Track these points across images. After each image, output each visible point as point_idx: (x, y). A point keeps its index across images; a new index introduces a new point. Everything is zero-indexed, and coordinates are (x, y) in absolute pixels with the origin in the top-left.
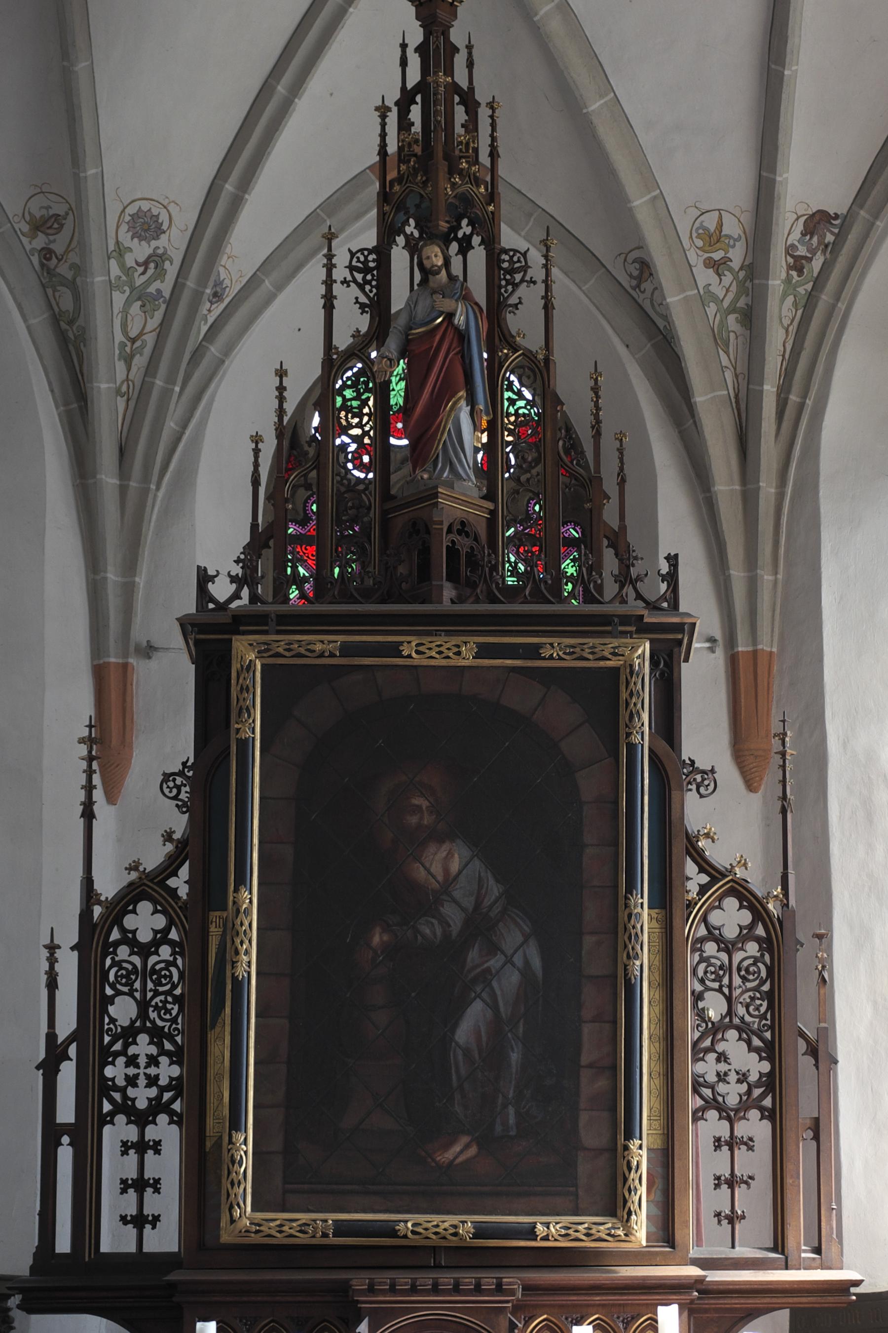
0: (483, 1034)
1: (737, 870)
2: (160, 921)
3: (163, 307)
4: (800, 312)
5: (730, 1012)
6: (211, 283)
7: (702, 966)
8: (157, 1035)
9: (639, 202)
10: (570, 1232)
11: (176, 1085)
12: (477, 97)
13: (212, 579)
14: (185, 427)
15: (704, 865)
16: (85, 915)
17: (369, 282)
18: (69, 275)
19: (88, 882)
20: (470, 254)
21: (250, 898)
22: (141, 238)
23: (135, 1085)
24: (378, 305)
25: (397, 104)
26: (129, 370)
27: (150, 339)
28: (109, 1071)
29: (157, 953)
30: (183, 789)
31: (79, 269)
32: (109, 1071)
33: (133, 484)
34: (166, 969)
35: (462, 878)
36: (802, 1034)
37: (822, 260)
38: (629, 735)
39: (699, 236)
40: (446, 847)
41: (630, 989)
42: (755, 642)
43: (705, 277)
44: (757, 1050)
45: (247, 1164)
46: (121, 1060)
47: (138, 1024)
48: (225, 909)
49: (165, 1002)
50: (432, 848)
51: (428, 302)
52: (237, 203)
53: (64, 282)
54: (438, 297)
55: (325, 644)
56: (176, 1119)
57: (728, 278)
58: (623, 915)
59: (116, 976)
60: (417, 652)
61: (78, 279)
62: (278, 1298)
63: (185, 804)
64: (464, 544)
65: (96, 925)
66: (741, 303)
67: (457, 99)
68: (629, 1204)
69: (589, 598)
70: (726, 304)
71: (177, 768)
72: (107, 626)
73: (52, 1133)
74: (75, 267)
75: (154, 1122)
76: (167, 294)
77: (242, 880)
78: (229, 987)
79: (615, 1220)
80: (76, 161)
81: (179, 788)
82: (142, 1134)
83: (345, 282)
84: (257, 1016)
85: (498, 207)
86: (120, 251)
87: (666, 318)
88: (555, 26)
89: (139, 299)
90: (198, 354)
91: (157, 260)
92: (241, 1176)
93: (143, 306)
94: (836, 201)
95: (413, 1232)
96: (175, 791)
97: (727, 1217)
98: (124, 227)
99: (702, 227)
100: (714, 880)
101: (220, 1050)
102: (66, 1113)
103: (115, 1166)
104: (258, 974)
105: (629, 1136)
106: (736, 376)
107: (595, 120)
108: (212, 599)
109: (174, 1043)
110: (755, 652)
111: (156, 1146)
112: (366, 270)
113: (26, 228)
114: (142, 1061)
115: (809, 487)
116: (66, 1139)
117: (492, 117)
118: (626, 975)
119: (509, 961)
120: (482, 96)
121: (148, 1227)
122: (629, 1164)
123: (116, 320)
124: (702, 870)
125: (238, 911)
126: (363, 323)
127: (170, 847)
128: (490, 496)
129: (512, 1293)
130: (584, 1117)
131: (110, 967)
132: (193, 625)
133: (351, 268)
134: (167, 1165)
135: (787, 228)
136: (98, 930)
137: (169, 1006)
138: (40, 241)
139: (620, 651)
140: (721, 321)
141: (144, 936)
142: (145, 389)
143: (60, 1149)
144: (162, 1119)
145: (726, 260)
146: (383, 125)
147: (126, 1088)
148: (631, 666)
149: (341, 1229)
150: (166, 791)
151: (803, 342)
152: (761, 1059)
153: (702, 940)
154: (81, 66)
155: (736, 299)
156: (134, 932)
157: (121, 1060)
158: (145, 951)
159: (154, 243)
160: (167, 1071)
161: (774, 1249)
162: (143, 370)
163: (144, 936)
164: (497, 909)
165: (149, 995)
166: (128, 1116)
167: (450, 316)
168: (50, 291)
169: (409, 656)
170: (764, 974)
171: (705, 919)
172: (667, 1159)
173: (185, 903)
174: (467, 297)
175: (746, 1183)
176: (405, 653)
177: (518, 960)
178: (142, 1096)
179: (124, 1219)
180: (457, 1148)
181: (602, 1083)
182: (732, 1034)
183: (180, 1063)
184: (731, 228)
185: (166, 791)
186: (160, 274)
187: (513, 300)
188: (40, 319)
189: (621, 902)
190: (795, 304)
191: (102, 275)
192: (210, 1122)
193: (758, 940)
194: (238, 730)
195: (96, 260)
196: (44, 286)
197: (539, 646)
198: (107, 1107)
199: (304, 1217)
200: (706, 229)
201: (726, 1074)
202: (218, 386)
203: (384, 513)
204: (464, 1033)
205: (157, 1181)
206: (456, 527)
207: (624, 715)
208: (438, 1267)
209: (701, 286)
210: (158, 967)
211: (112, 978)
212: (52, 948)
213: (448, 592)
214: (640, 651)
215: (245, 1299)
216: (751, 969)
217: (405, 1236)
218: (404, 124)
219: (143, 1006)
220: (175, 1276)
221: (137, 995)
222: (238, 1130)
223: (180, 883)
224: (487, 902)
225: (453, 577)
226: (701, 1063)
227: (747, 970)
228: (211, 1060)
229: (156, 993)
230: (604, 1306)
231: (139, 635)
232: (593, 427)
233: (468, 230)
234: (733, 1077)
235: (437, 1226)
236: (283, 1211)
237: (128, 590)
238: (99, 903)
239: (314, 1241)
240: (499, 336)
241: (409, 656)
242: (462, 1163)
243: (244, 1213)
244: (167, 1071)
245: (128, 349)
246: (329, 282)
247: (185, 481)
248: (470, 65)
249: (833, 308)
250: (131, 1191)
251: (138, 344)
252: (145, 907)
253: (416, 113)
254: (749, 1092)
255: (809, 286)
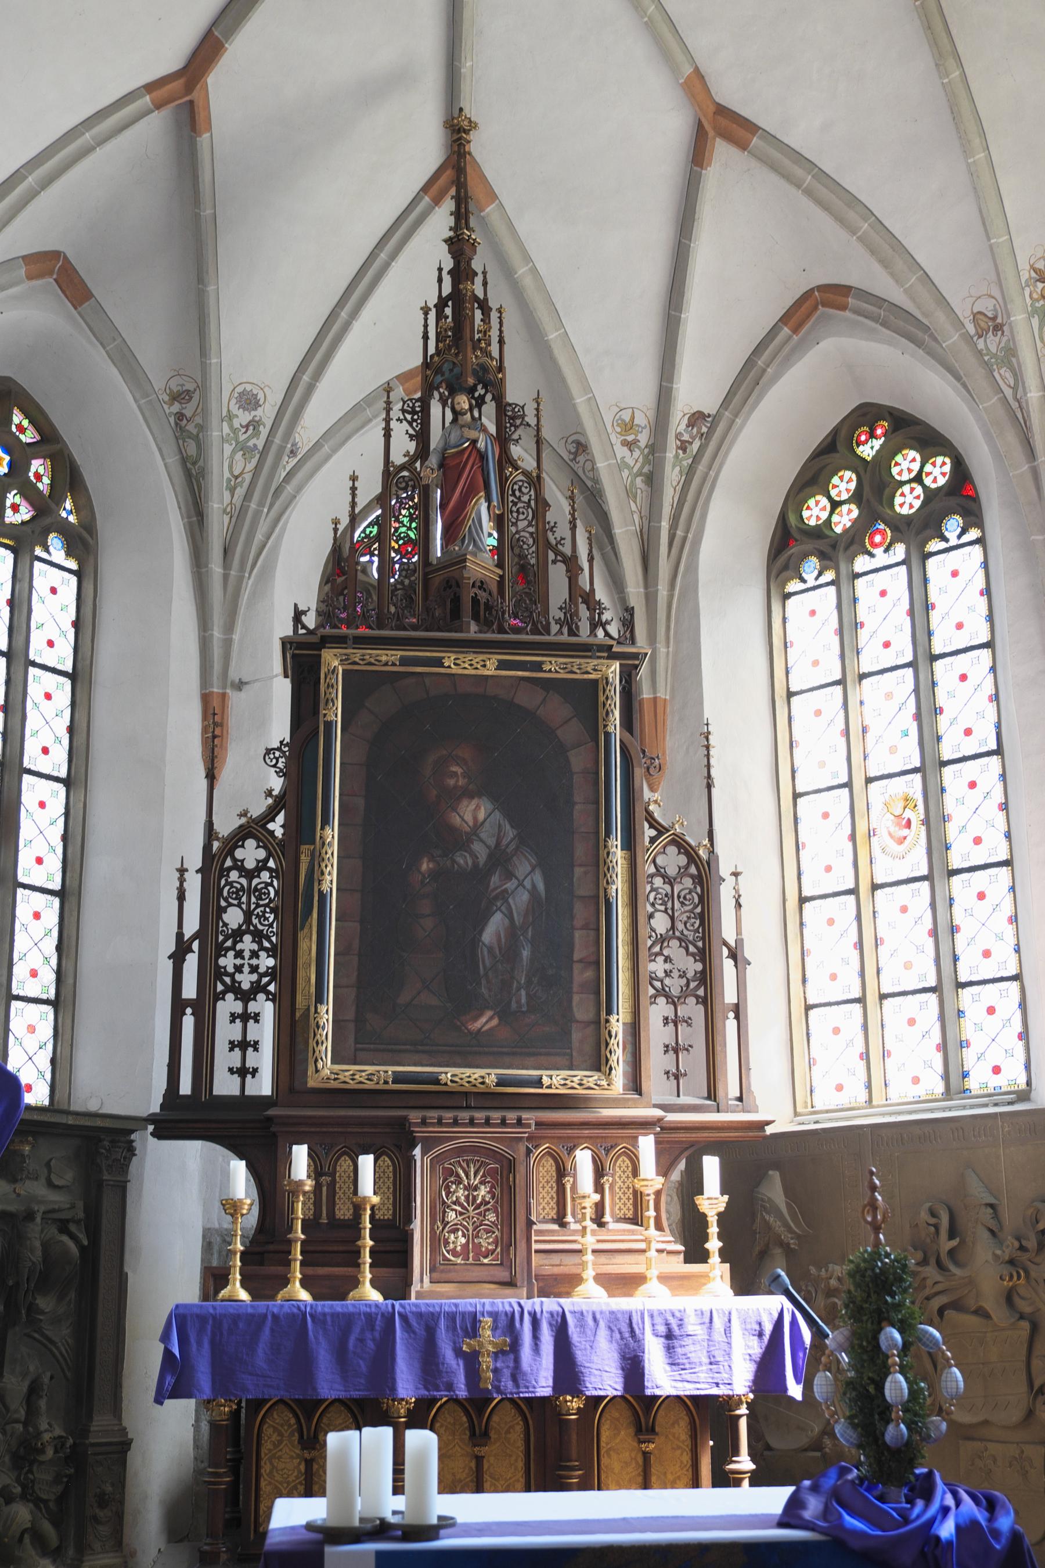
0: (502, 936)
1: (677, 826)
2: (262, 854)
3: (258, 456)
4: (683, 478)
5: (673, 927)
6: (291, 441)
7: (653, 895)
8: (258, 936)
9: (580, 400)
10: (568, 1082)
11: (272, 973)
12: (490, 304)
13: (304, 613)
14: (268, 538)
15: (653, 824)
16: (207, 848)
17: (416, 421)
18: (195, 432)
19: (209, 825)
20: (484, 408)
21: (332, 834)
22: (244, 409)
23: (241, 972)
24: (422, 437)
25: (435, 306)
26: (232, 497)
27: (248, 477)
28: (222, 961)
29: (259, 876)
30: (281, 760)
31: (201, 428)
32: (222, 961)
33: (232, 573)
34: (266, 888)
35: (487, 824)
36: (725, 944)
37: (699, 444)
38: (605, 726)
39: (618, 425)
40: (475, 802)
41: (608, 905)
42: (655, 692)
43: (622, 452)
44: (693, 955)
45: (329, 1028)
46: (231, 954)
47: (244, 927)
48: (313, 843)
49: (265, 912)
50: (465, 802)
51: (459, 432)
52: (310, 389)
53: (191, 436)
54: (466, 430)
55: (389, 657)
56: (272, 997)
57: (637, 453)
58: (603, 853)
59: (229, 892)
60: (455, 664)
61: (201, 435)
62: (349, 1130)
63: (281, 770)
64: (483, 596)
65: (215, 855)
66: (645, 470)
67: (476, 305)
68: (610, 1062)
69: (572, 633)
70: (635, 470)
71: (276, 745)
72: (212, 667)
73: (178, 1006)
74: (197, 426)
75: (255, 999)
76: (260, 448)
77: (326, 821)
78: (316, 898)
79: (599, 1074)
80: (204, 352)
81: (277, 759)
82: (246, 1008)
83: (398, 420)
84: (336, 920)
85: (504, 375)
86: (230, 417)
87: (597, 481)
88: (528, 282)
89: (241, 449)
90: (279, 490)
91: (254, 425)
92: (324, 1037)
93: (244, 454)
94: (710, 406)
95: (452, 1081)
96: (274, 761)
97: (673, 1074)
98: (233, 401)
99: (620, 419)
100: (660, 834)
101: (308, 946)
102: (190, 991)
103: (226, 1031)
104: (337, 889)
105: (609, 1012)
106: (641, 518)
107: (553, 346)
108: (304, 627)
109: (270, 942)
110: (655, 699)
111: (256, 1017)
112: (413, 412)
113: (166, 398)
114: (247, 954)
115: (691, 589)
116: (189, 1011)
117: (500, 318)
118: (606, 896)
119: (521, 884)
120: (493, 304)
121: (249, 1076)
122: (610, 1032)
123: (225, 463)
124: (651, 826)
125: (324, 844)
126: (412, 447)
127: (270, 801)
128: (500, 565)
129: (529, 1126)
130: (576, 998)
131: (225, 886)
132: (291, 643)
133: (403, 411)
134: (265, 1032)
135: (678, 422)
136: (216, 860)
137: (267, 915)
138: (176, 408)
139: (599, 668)
140: (632, 481)
141: (250, 864)
142: (243, 510)
143: (185, 1018)
144: (261, 997)
145: (635, 442)
146: (426, 320)
147: (234, 974)
148: (607, 679)
149: (398, 1078)
150: (268, 761)
151: (686, 496)
152: (696, 961)
153: (652, 876)
154: (211, 288)
155: (642, 467)
156: (242, 861)
157: (231, 954)
158: (250, 875)
159: (253, 413)
160: (267, 962)
161: (709, 1098)
162: (242, 498)
163: (250, 864)
164: (512, 846)
165: (253, 906)
166: (235, 994)
167: (474, 442)
168: (181, 442)
169: (449, 667)
170: (696, 900)
171: (654, 861)
172: (635, 1029)
173: (281, 840)
174: (484, 430)
175: (687, 1050)
176: (446, 664)
177: (527, 883)
178: (246, 980)
179: (231, 1070)
180: (484, 1020)
181: (589, 974)
182: (674, 943)
183: (274, 956)
184: (640, 420)
185: (268, 761)
186: (257, 434)
187: (515, 436)
188: (173, 460)
189: (602, 844)
190: (681, 472)
191: (217, 431)
192: (299, 998)
193: (692, 876)
194: (325, 715)
195: (214, 421)
196: (177, 438)
197: (542, 663)
198: (220, 987)
199: (370, 1069)
200: (623, 420)
201: (671, 971)
202: (291, 513)
203: (426, 574)
204: (488, 936)
205: (256, 1043)
206: (478, 584)
207: (602, 713)
208: (468, 1107)
209: (619, 457)
210: (259, 887)
211: (225, 894)
212: (182, 871)
213: (474, 627)
214: (613, 669)
215: (324, 1130)
216: (688, 897)
217: (446, 1084)
218: (440, 315)
219: (248, 915)
220: (271, 1112)
221: (244, 906)
222: (321, 1003)
223: (277, 827)
224: (505, 842)
225: (476, 617)
226: (653, 963)
227: (685, 898)
228: (300, 953)
229: (258, 906)
230: (591, 1137)
231: (234, 675)
232: (570, 522)
233: (482, 392)
234: (675, 974)
235: (469, 1077)
236: (355, 1064)
237: (228, 644)
238: (218, 839)
239: (378, 1087)
240: (505, 460)
241: (449, 667)
242: (486, 1031)
243: (326, 1067)
244: (267, 962)
245: (232, 483)
246: (388, 420)
247: (267, 574)
248: (485, 284)
249: (707, 474)
250: (237, 1050)
251: (239, 480)
252: (250, 843)
253: (448, 311)
254: (688, 985)
255: (690, 461)
